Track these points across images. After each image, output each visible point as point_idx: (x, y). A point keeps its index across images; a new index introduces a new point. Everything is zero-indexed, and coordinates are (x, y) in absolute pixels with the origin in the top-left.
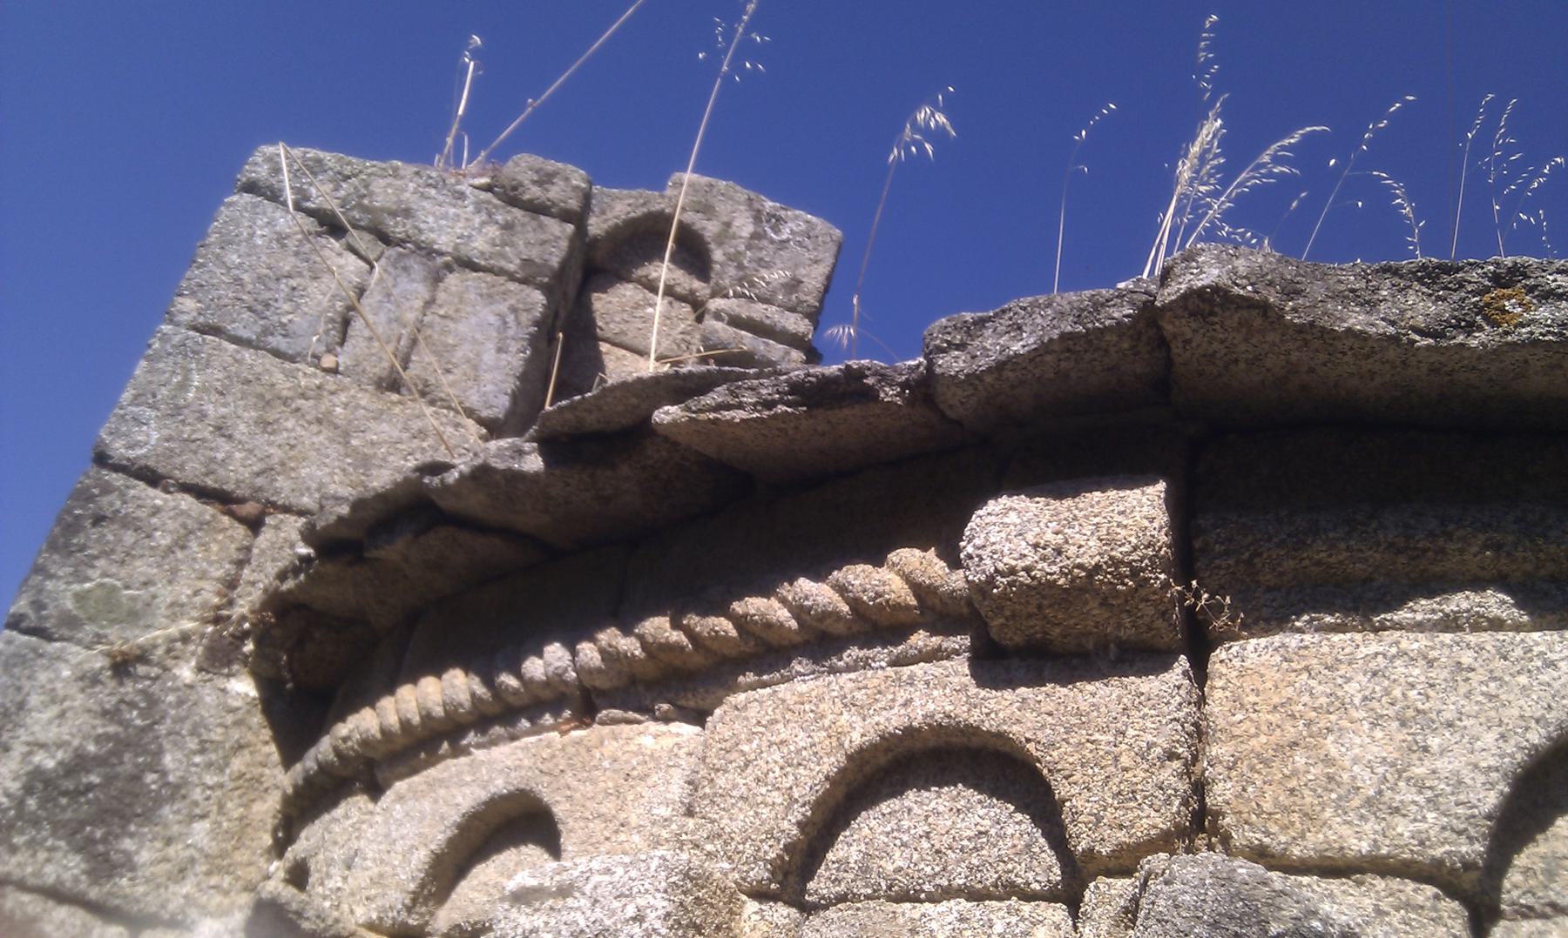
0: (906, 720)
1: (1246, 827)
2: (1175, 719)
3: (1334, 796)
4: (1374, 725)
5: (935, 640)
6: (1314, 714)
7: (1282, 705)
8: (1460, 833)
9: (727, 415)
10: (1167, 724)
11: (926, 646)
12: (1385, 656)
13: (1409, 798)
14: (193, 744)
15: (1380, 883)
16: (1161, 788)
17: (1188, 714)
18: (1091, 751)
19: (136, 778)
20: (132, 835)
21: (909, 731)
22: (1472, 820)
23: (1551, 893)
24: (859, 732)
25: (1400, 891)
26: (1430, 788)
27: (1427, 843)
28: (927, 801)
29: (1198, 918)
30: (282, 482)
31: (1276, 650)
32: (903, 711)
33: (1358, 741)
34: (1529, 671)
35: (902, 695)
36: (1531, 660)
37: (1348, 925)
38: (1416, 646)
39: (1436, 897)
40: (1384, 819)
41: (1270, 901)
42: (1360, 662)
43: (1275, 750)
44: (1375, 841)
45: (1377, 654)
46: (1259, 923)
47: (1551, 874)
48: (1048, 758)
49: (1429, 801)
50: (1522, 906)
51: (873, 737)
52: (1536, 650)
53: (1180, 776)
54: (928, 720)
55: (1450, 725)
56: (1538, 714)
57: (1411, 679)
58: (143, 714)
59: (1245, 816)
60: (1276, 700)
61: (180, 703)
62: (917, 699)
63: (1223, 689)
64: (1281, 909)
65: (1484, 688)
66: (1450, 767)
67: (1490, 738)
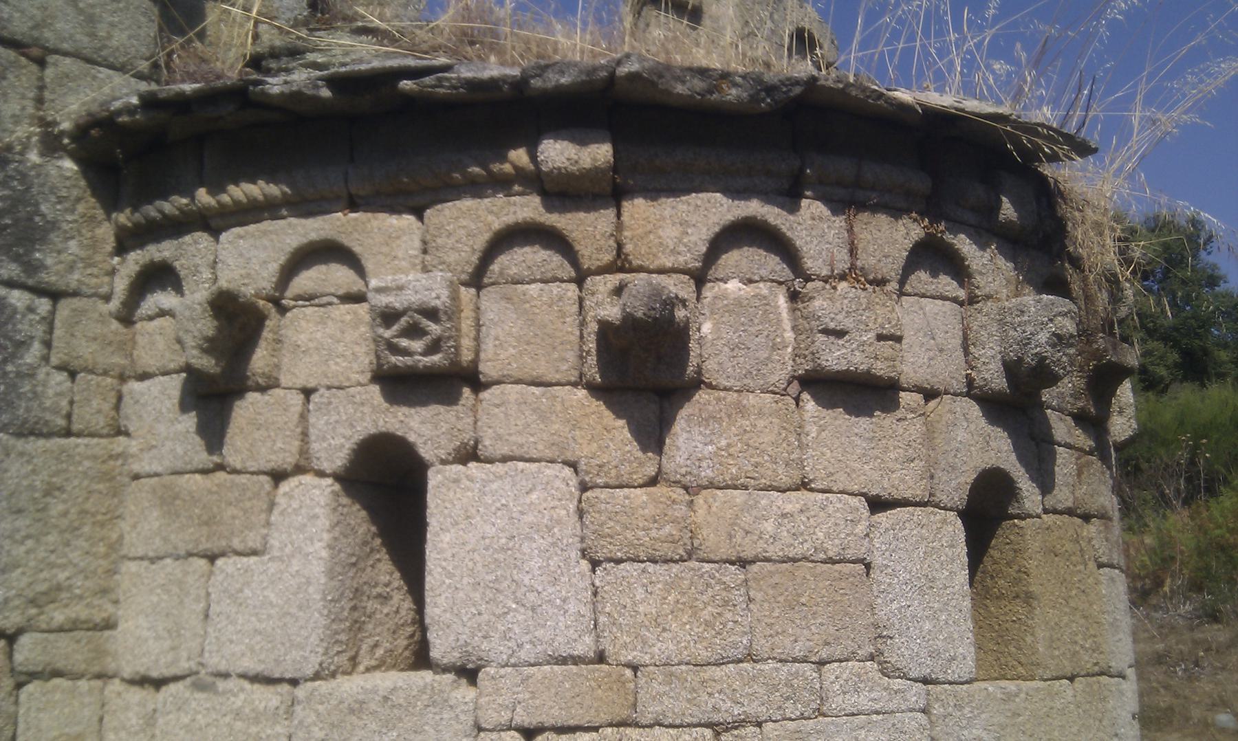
9: (438, 90)
14: (53, 199)
19: (30, 219)
20: (39, 250)
21: (517, 224)
24: (497, 225)
30: (47, 34)
35: (512, 209)
51: (503, 226)
58: (22, 182)
61: (38, 175)
67: (705, 230)
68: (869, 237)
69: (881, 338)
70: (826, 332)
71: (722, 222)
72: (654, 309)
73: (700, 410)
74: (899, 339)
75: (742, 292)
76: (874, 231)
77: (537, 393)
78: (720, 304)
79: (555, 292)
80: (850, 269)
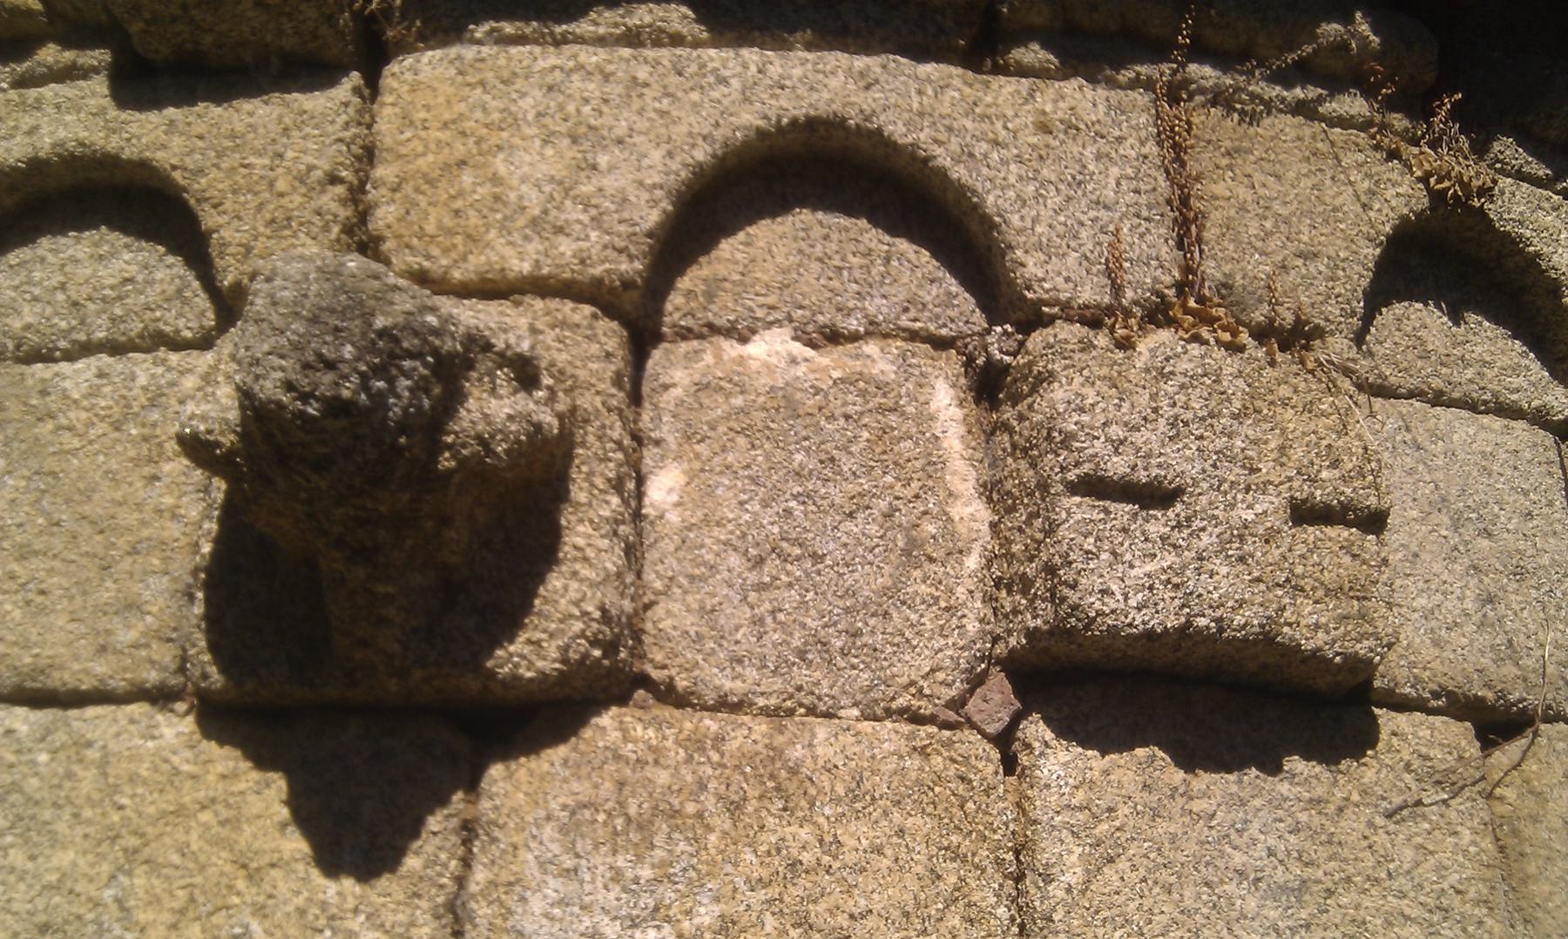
0: (30, 150)
1: (407, 251)
2: (340, 140)
3: (499, 216)
4: (545, 142)
5: (69, 56)
6: (485, 131)
7: (454, 121)
8: (620, 251)
10: (331, 145)
11: (57, 62)
12: (562, 69)
13: (574, 216)
15: (539, 304)
16: (319, 214)
17: (356, 136)
18: (244, 177)
21: (36, 165)
22: (633, 238)
23: (710, 314)
25: (557, 310)
26: (596, 207)
27: (588, 262)
28: (64, 248)
29: (297, 313)
31: (451, 62)
32: (27, 140)
33: (527, 158)
34: (702, 88)
35: (27, 121)
36: (705, 76)
37: (477, 328)
38: (594, 59)
39: (595, 316)
40: (547, 239)
41: (379, 295)
42: (537, 75)
43: (441, 169)
44: (537, 261)
45: (554, 67)
46: (363, 315)
47: (710, 296)
48: (196, 186)
49: (593, 219)
50: (682, 327)
52: (710, 65)
53: (343, 202)
54: (58, 150)
55: (620, 142)
56: (705, 132)
57: (586, 94)
59: (406, 239)
60: (447, 116)
62: (45, 126)
63: (393, 105)
64: (392, 303)
65: (657, 105)
66: (616, 184)
67: (657, 156)
68: (1243, 192)
69: (1304, 513)
70: (1096, 487)
71: (718, 134)
72: (330, 365)
73: (621, 784)
74: (1374, 522)
75: (801, 370)
76: (1258, 177)
77: (23, 729)
78: (718, 408)
79: (142, 380)
80: (1181, 287)
